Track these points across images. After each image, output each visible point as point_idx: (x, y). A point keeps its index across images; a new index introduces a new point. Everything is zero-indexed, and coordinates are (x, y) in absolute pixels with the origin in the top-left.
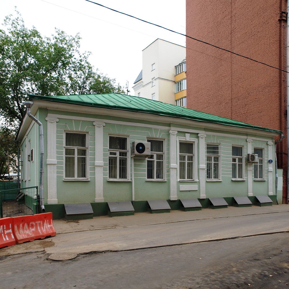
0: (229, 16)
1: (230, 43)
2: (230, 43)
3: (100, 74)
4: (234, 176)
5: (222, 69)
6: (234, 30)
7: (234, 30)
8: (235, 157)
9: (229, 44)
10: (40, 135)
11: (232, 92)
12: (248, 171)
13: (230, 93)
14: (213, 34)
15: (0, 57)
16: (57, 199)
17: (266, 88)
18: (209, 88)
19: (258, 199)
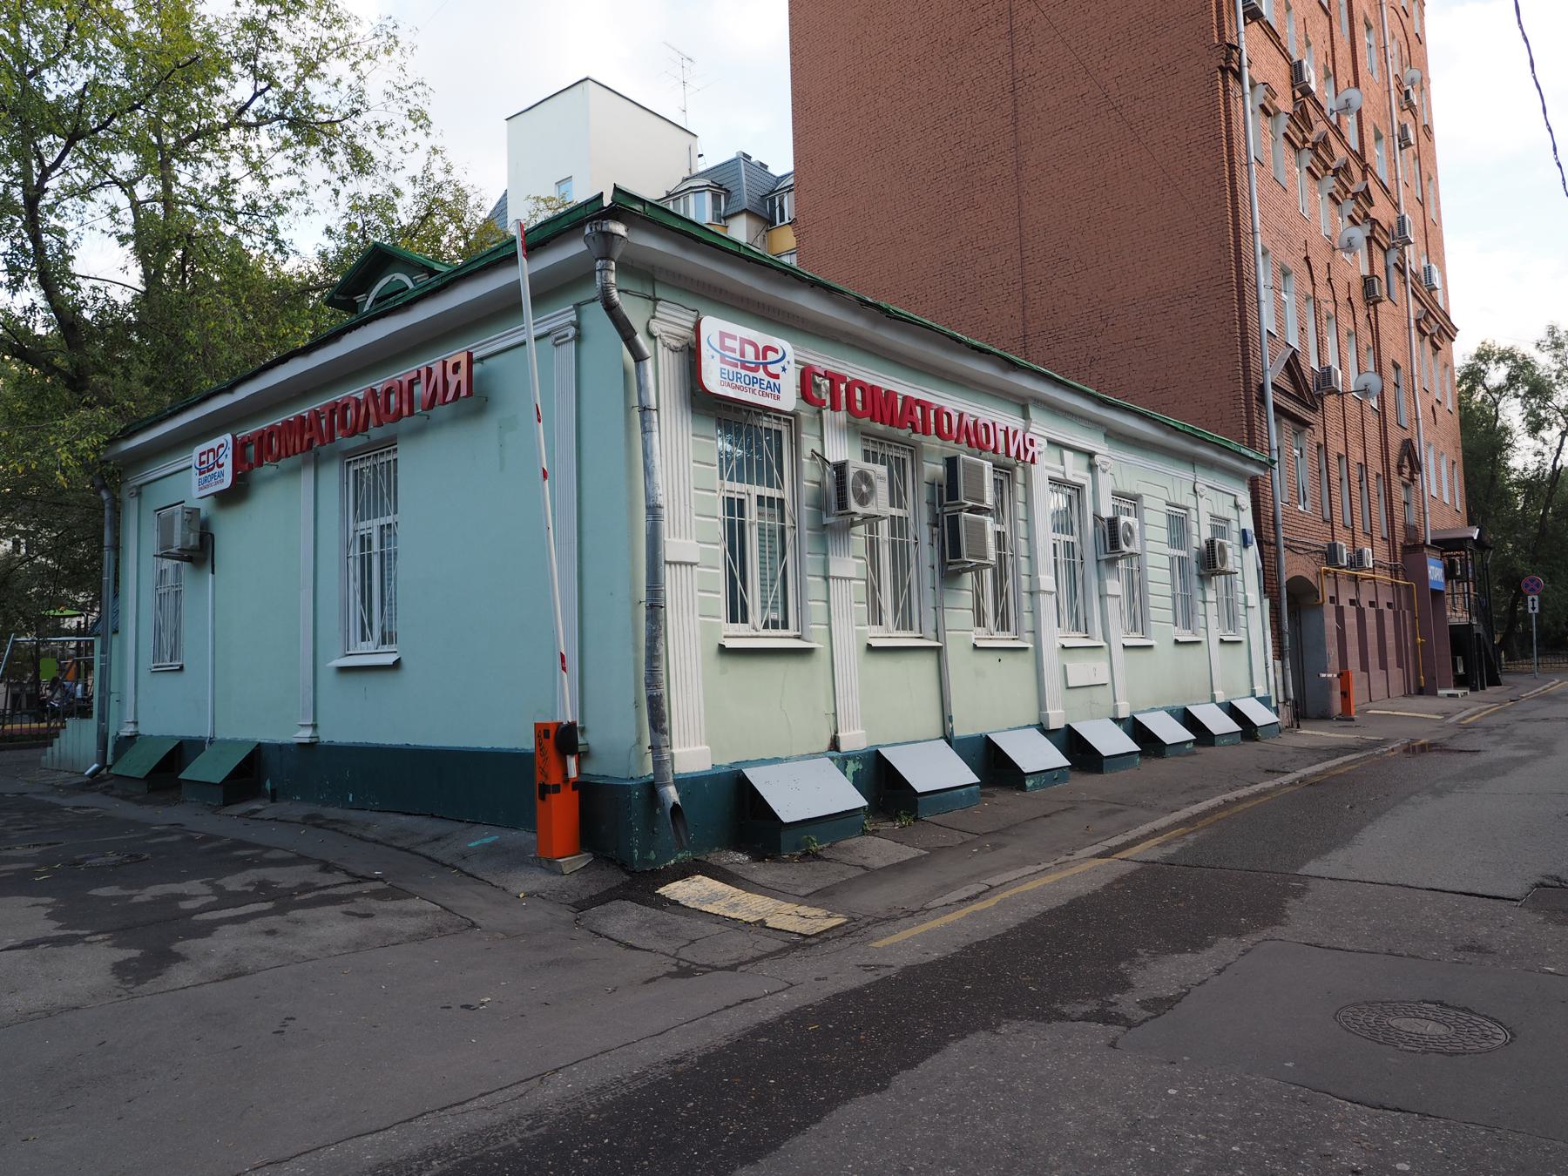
0: (1004, 29)
1: (1011, 127)
2: (1011, 127)
3: (347, 190)
4: (737, 612)
5: (974, 219)
6: (1028, 81)
7: (1026, 80)
8: (738, 488)
9: (1008, 129)
10: (1033, 632)
11: (1028, 312)
12: (831, 580)
13: (1018, 315)
14: (926, 83)
15: (3, 148)
16: (707, 747)
17: (1182, 302)
18: (915, 292)
19: (157, 760)
